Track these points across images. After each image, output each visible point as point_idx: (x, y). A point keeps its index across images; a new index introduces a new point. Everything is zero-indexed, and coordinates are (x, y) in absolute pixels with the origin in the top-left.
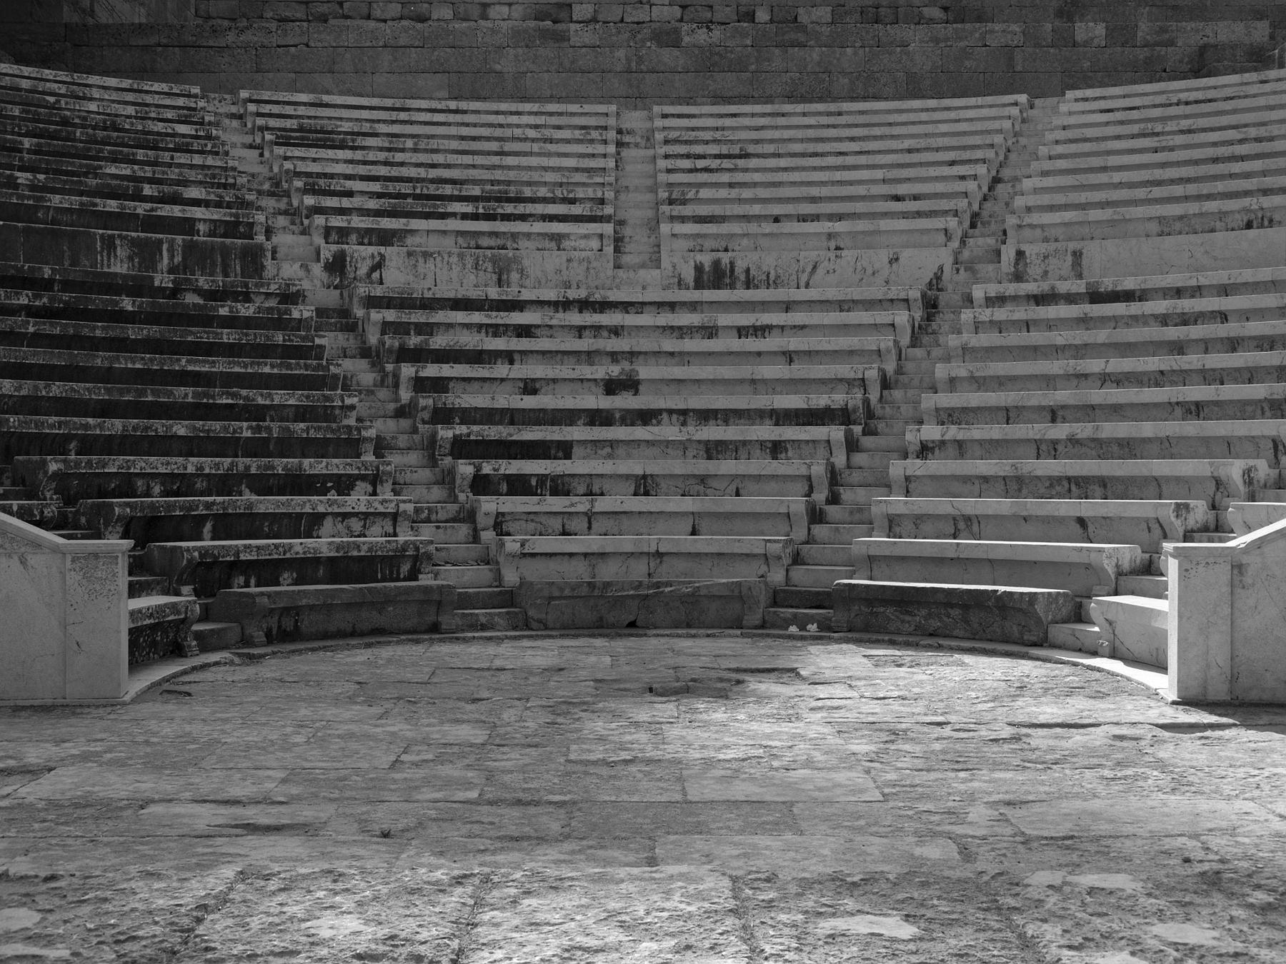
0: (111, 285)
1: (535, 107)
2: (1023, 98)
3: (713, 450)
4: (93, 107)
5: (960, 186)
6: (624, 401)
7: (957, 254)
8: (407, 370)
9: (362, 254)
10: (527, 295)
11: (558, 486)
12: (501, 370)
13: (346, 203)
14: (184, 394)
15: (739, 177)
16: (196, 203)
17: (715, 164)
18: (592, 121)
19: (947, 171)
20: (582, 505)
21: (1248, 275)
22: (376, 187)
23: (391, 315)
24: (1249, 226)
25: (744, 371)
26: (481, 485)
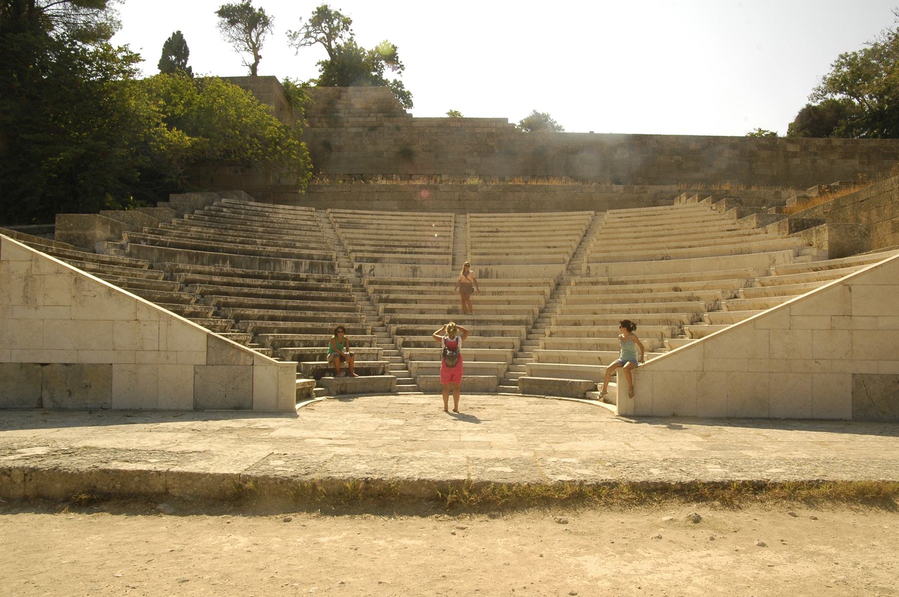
0: (286, 278)
1: (427, 214)
2: (593, 213)
4: (280, 216)
5: (569, 243)
7: (568, 266)
9: (367, 267)
10: (422, 280)
12: (413, 306)
13: (362, 248)
14: (310, 314)
15: (495, 239)
16: (313, 249)
17: (487, 234)
18: (447, 219)
19: (564, 238)
21: (659, 277)
22: (372, 242)
24: (663, 259)
25: (494, 307)
26: (406, 344)
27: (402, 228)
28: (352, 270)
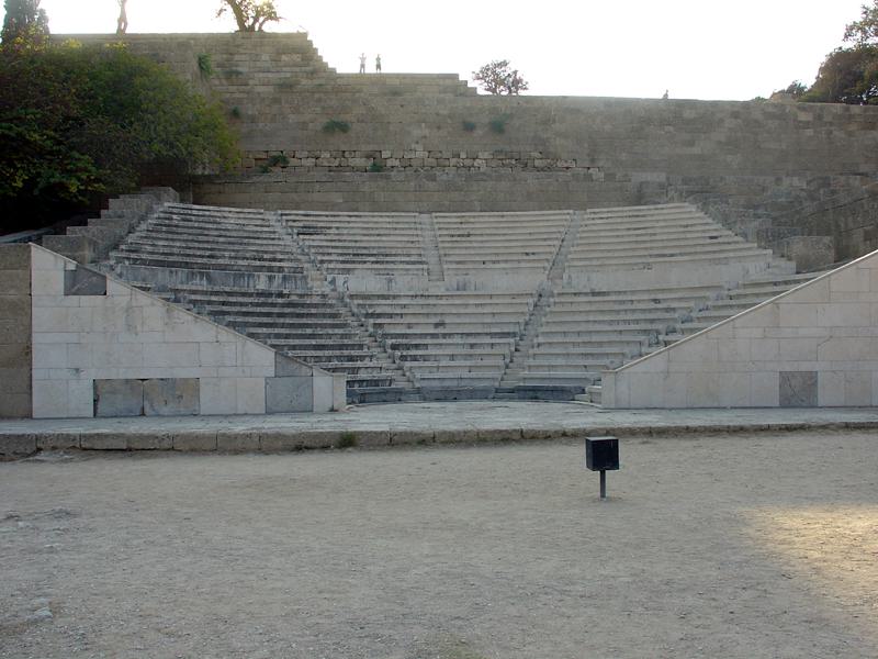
2: (571, 211)
3: (472, 346)
5: (548, 250)
6: (440, 330)
8: (371, 321)
11: (425, 358)
12: (398, 320)
14: (309, 331)
20: (436, 364)
23: (361, 302)
26: (403, 358)
27: (365, 232)
28: (326, 283)
